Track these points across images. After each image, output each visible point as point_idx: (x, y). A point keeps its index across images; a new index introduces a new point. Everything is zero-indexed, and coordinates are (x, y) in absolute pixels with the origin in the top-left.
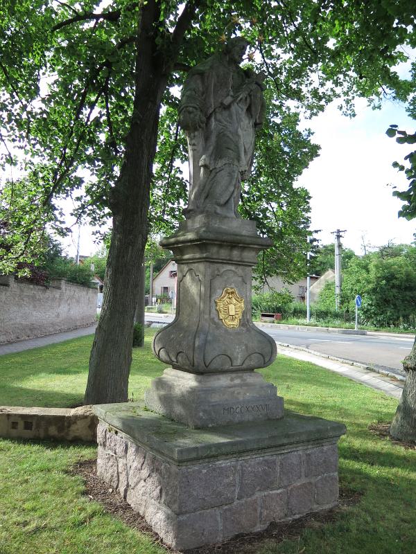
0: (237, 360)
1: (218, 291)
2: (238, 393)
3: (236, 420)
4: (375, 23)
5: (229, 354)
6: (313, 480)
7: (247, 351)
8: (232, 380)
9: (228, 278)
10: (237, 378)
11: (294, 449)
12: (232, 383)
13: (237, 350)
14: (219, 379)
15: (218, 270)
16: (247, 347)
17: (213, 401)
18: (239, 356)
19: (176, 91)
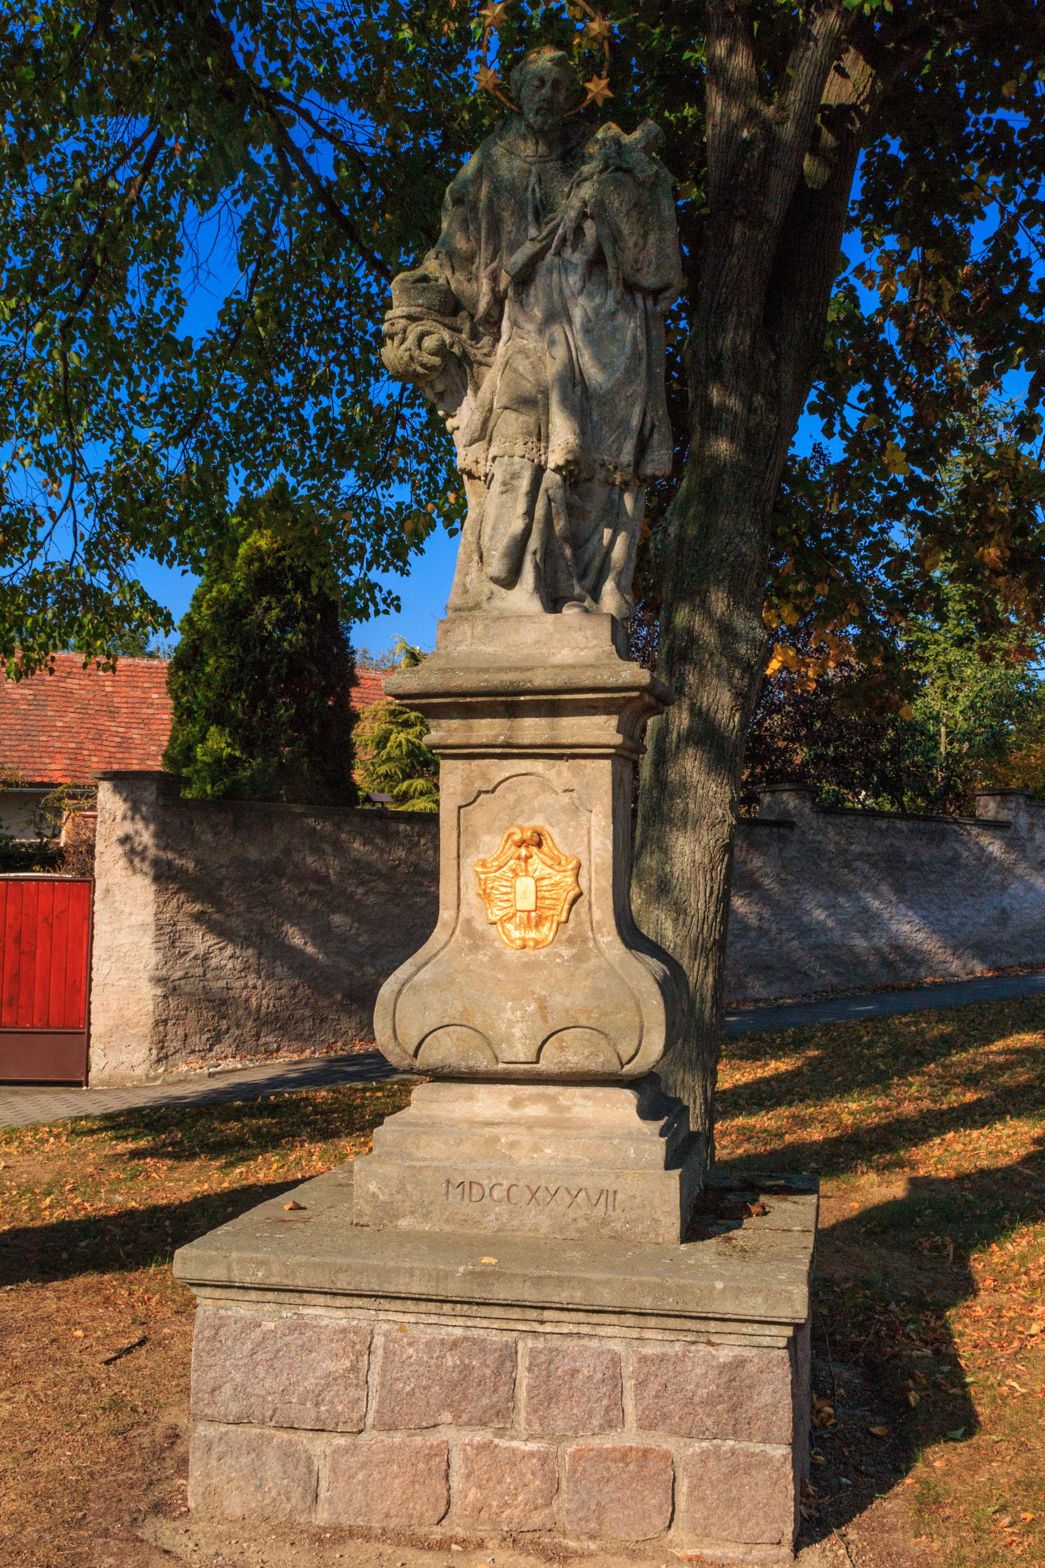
0: (511, 1046)
1: (486, 838)
2: (513, 1145)
3: (490, 1224)
4: (237, 441)
5: (478, 1022)
6: (670, 1444)
7: (545, 1019)
8: (516, 1103)
9: (519, 800)
10: (534, 1099)
11: (585, 1329)
12: (515, 1114)
13: (509, 1015)
14: (471, 1098)
15: (484, 776)
16: (543, 1007)
17: (421, 1153)
18: (517, 1032)
19: (634, 61)
